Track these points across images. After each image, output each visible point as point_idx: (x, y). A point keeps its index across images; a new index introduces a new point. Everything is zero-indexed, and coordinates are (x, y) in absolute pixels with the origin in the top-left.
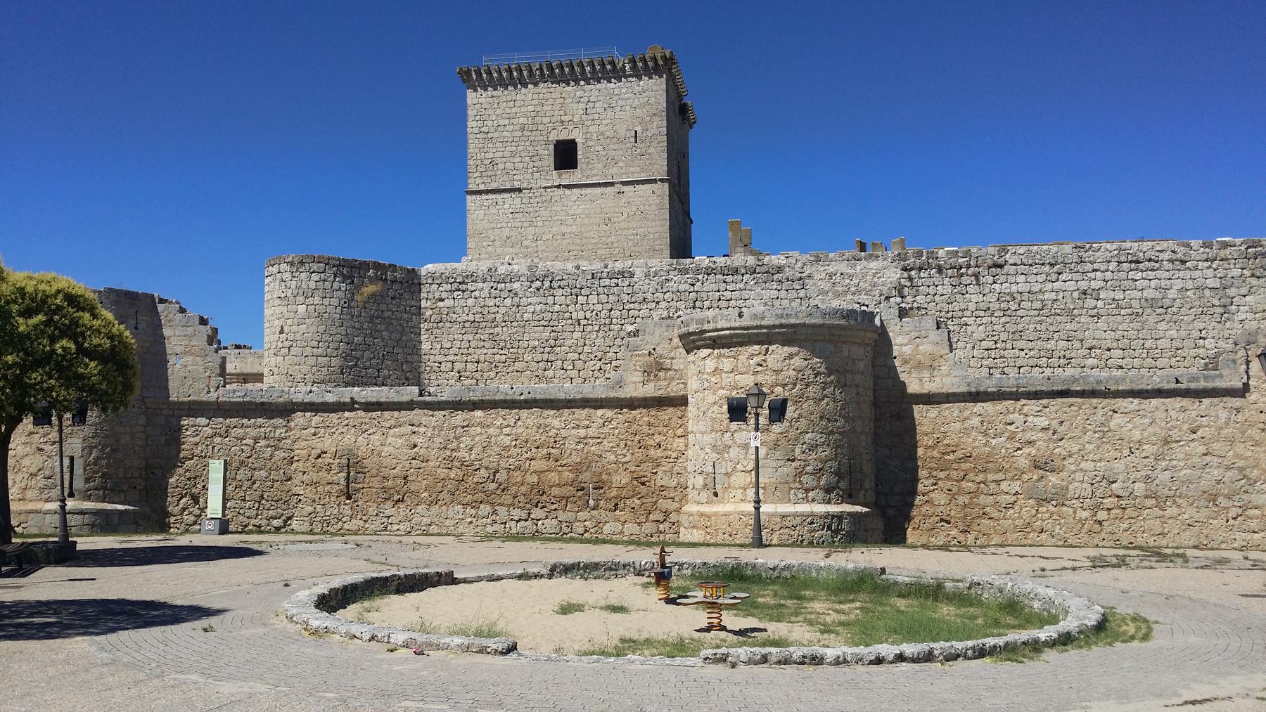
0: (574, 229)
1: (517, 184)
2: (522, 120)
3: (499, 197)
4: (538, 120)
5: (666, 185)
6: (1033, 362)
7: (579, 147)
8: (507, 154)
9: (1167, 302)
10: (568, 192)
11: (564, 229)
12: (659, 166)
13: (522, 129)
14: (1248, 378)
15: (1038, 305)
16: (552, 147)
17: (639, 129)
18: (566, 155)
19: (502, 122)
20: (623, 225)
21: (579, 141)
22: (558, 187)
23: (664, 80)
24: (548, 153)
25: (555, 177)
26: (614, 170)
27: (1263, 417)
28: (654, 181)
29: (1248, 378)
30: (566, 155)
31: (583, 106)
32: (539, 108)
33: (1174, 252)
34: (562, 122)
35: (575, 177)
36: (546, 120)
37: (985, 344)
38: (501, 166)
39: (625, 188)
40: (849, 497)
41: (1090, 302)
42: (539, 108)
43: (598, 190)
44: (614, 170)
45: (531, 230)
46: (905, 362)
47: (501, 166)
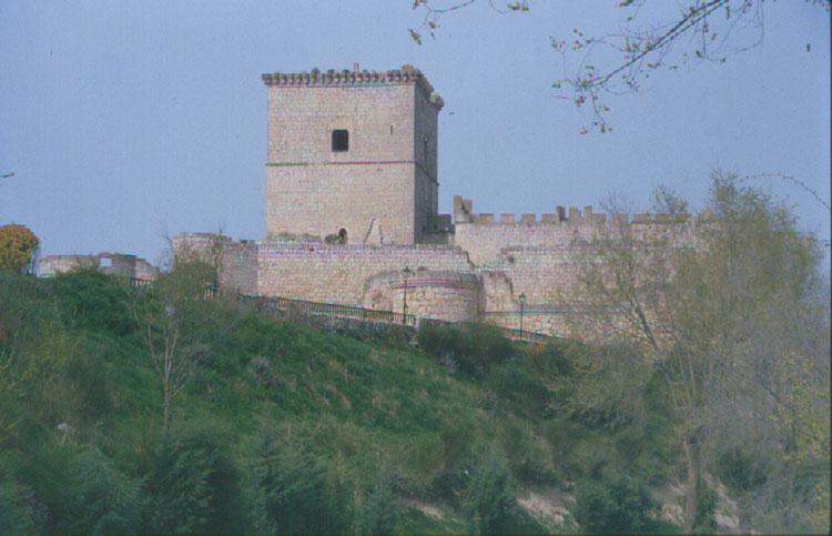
2: (309, 114)
3: (291, 169)
5: (413, 165)
7: (337, 128)
10: (340, 166)
12: (409, 152)
14: (712, 60)
16: (330, 135)
17: (394, 124)
18: (340, 141)
21: (351, 131)
22: (334, 163)
23: (412, 87)
24: (328, 139)
25: (333, 156)
27: (755, 4)
28: (404, 162)
29: (712, 60)
30: (340, 141)
33: (742, 181)
34: (338, 117)
35: (341, 156)
36: (326, 114)
38: (292, 147)
39: (383, 167)
43: (363, 167)
45: (313, 195)
46: (491, 297)
47: (292, 147)
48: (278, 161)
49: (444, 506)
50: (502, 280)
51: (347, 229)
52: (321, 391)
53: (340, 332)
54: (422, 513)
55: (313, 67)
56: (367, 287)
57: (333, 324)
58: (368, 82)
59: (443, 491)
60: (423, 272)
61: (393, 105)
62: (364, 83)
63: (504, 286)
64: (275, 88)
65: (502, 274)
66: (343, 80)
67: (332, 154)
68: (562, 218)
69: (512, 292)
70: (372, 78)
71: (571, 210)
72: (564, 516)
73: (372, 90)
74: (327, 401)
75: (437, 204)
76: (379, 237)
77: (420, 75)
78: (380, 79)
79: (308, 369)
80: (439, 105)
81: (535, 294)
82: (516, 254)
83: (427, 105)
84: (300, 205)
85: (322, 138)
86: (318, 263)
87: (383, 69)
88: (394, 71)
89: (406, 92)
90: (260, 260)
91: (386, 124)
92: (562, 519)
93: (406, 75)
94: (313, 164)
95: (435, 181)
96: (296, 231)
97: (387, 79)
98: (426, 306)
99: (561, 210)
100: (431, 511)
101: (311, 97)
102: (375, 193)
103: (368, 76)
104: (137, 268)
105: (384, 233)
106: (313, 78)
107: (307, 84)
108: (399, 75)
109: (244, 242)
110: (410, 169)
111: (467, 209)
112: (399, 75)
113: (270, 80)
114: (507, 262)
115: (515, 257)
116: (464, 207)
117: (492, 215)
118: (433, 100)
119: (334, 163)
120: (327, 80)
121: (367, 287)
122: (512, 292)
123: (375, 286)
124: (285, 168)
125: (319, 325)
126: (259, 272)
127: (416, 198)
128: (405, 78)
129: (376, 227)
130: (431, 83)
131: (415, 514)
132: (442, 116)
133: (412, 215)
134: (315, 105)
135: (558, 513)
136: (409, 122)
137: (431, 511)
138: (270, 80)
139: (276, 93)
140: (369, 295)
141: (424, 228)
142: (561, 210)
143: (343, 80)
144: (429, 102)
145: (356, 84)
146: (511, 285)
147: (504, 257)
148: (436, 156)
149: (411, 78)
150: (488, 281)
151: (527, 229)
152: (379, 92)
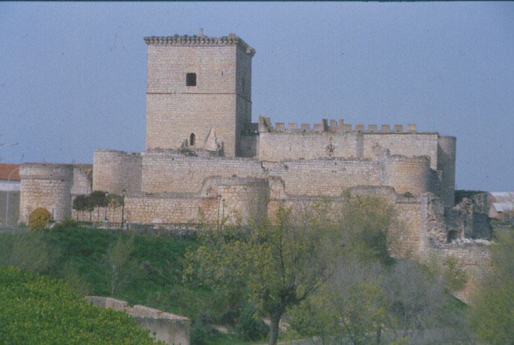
0: (194, 113)
1: (169, 91)
2: (172, 62)
4: (179, 63)
5: (235, 96)
8: (165, 77)
13: (172, 67)
16: (185, 76)
17: (224, 70)
18: (191, 80)
19: (163, 63)
20: (216, 112)
21: (198, 74)
22: (188, 93)
23: (235, 48)
24: (184, 79)
30: (191, 80)
31: (199, 58)
35: (192, 89)
39: (218, 96)
41: (334, 174)
45: (175, 112)
48: (153, 91)
49: (228, 326)
50: (279, 181)
51: (195, 134)
52: (174, 273)
53: (184, 237)
54: (218, 331)
55: (175, 33)
56: (204, 183)
57: (180, 233)
58: (208, 43)
59: (228, 320)
60: (235, 178)
61: (223, 58)
62: (206, 44)
63: (280, 184)
64: (151, 46)
65: (279, 178)
66: (193, 42)
67: (186, 87)
68: (326, 129)
69: (284, 187)
70: (210, 41)
71: (331, 121)
72: (287, 327)
73: (210, 49)
74: (176, 278)
75: (251, 110)
76: (215, 138)
77: (240, 40)
78: (216, 42)
79: (168, 262)
80: (252, 53)
81: (299, 187)
82: (289, 164)
83: (244, 53)
84: (167, 118)
85: (181, 77)
86: (177, 167)
87: (218, 35)
88: (224, 37)
89: (230, 51)
90: (143, 164)
91: (219, 70)
92: (285, 328)
93: (231, 40)
94: (175, 93)
95: (250, 101)
96: (164, 146)
97: (219, 42)
98: (231, 208)
99: (325, 121)
100: (223, 330)
101: (174, 51)
102: (213, 114)
103: (209, 40)
104: (74, 172)
105: (217, 136)
106: (174, 40)
107: (171, 43)
108: (227, 40)
109: (134, 154)
110: (233, 98)
111: (267, 123)
112: (227, 40)
113: (150, 40)
114: (284, 169)
115: (288, 166)
116: (266, 123)
117: (284, 124)
118: (248, 51)
119: (188, 93)
120: (183, 42)
121: (204, 183)
122: (284, 187)
123: (208, 184)
124: (158, 95)
125: (173, 235)
126: (143, 171)
127: (237, 115)
128: (230, 42)
129: (212, 134)
130: (246, 42)
131: (214, 331)
132: (254, 60)
133: (234, 126)
135: (284, 326)
136: (232, 71)
137: (223, 330)
138: (150, 40)
139: (152, 50)
140: (205, 189)
141: (243, 132)
142: (325, 121)
143: (193, 42)
144: (246, 54)
145: (201, 44)
146: (284, 185)
147: (282, 165)
148: (250, 86)
149: (235, 42)
150: (271, 182)
151: (302, 136)
152: (215, 49)
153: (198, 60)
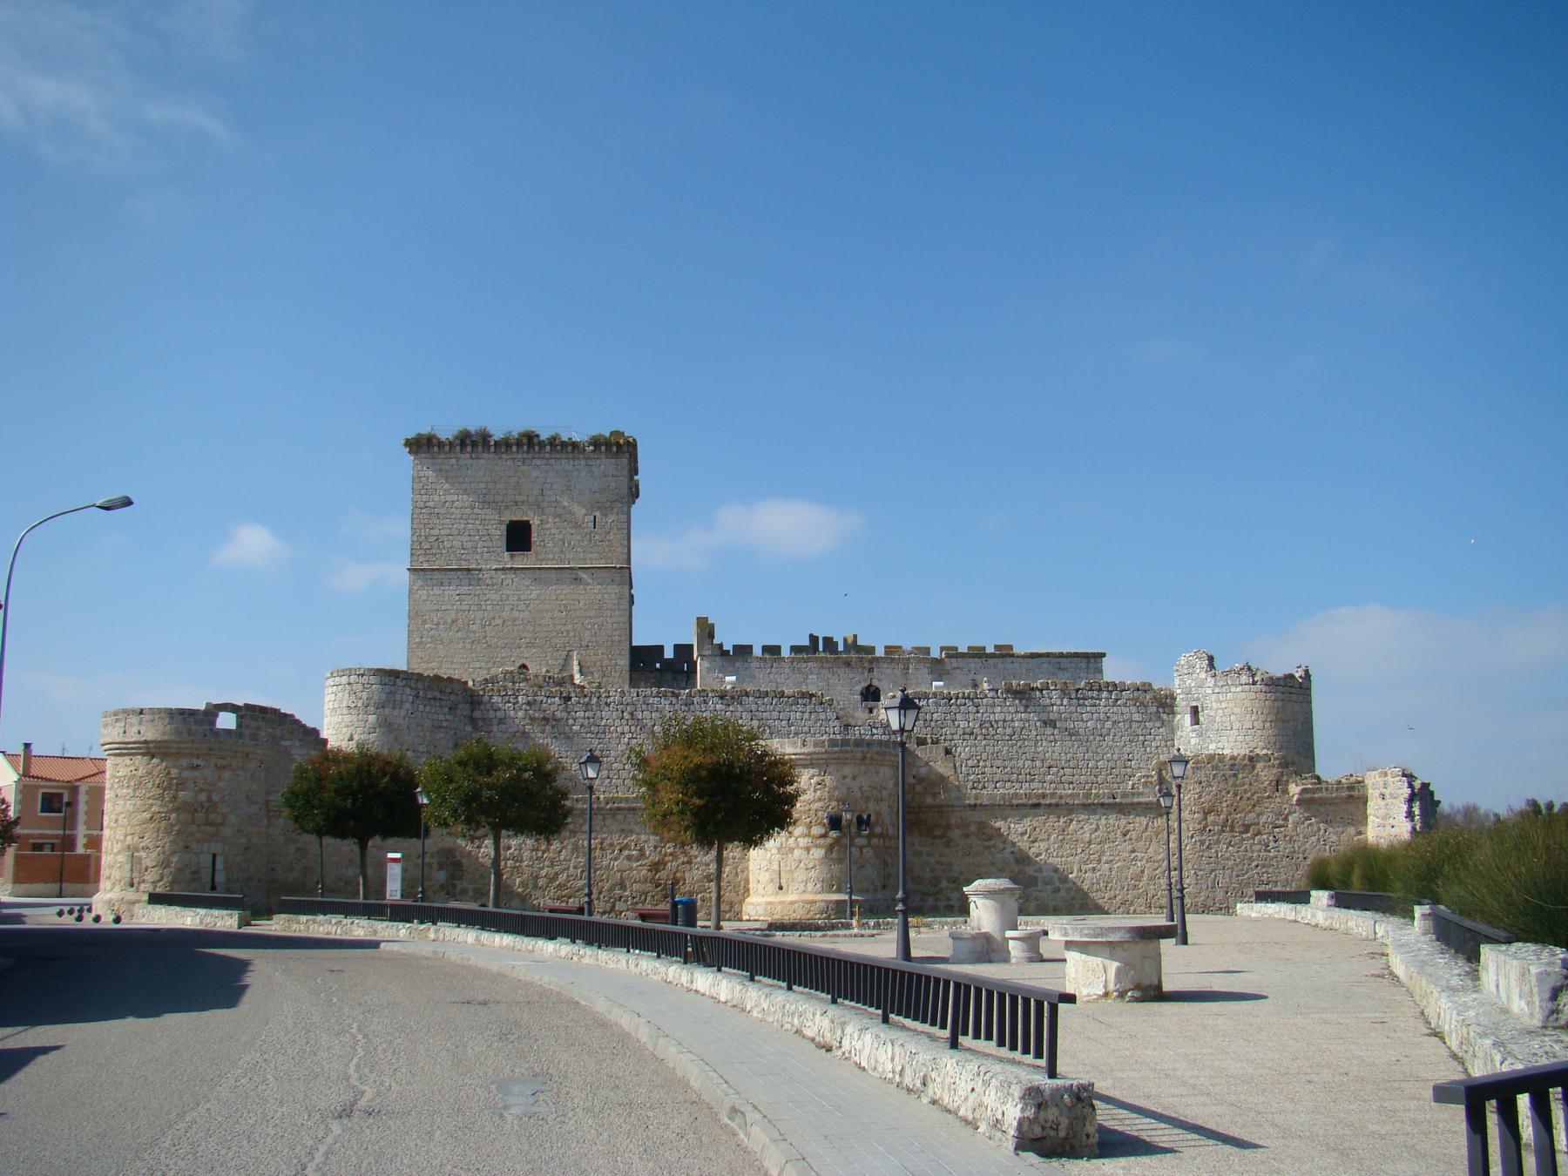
6: (1006, 778)
7: (534, 528)
9: (1104, 731)
11: (515, 614)
15: (1009, 731)
16: (504, 527)
18: (518, 537)
21: (535, 522)
24: (499, 534)
26: (570, 556)
30: (518, 537)
32: (491, 486)
35: (522, 560)
37: (970, 763)
40: (839, 891)
42: (491, 486)
44: (570, 556)
113: (127, 502)
134: (482, 485)
153: (536, 492)
